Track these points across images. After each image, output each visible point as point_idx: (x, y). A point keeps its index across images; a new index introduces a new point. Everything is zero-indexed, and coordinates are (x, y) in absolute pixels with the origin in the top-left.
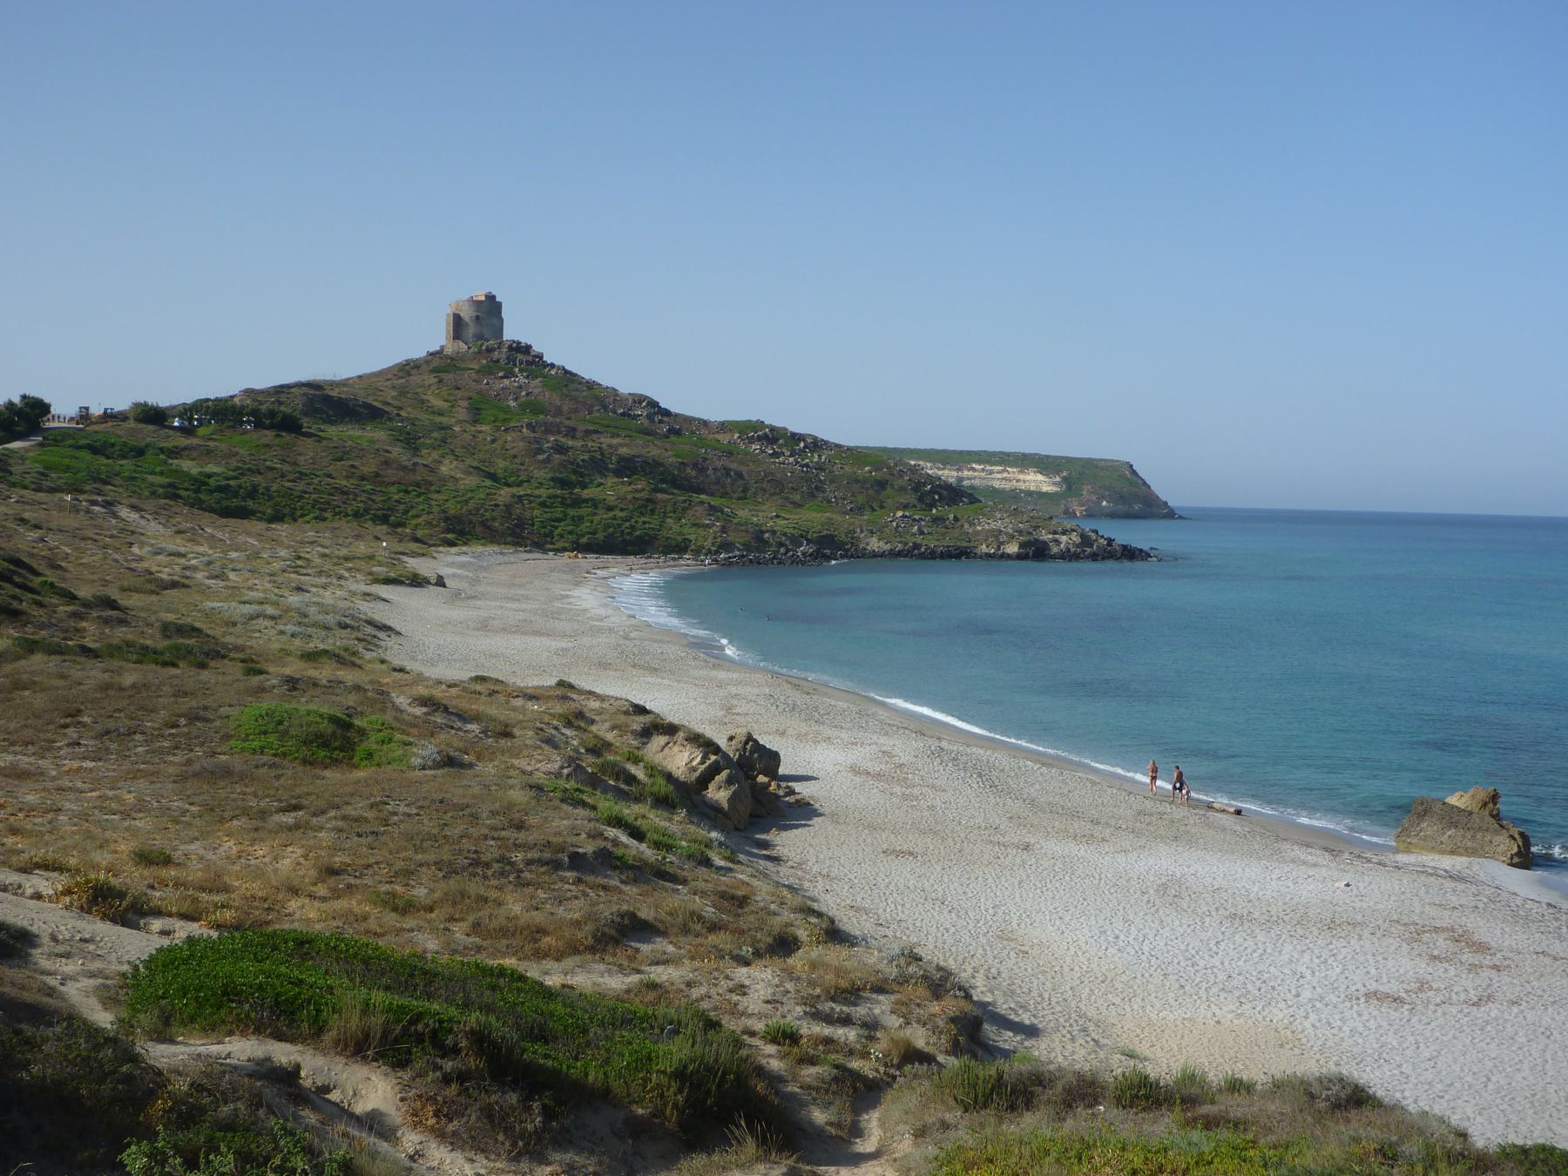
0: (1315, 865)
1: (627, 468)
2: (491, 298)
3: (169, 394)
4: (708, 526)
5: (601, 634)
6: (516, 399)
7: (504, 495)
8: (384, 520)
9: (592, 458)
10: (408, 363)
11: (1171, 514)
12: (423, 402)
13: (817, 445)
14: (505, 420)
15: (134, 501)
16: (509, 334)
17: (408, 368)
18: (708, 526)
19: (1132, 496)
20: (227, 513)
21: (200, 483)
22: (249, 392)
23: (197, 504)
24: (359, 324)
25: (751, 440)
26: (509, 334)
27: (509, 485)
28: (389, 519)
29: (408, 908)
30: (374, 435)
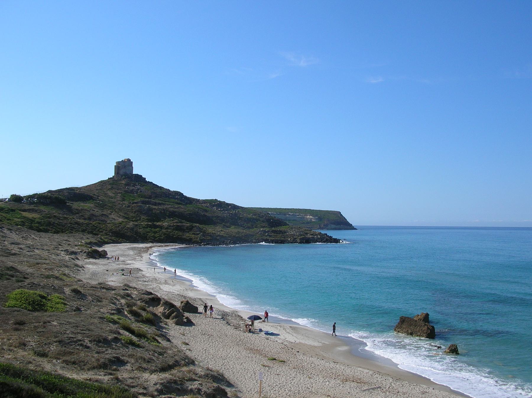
0: (48, 277)
1: (173, 215)
2: (129, 160)
3: (24, 192)
4: (198, 234)
5: (153, 268)
6: (137, 193)
7: (131, 224)
8: (91, 233)
9: (161, 212)
10: (102, 182)
11: (355, 229)
12: (106, 194)
13: (234, 207)
14: (133, 200)
15: (9, 227)
16: (135, 172)
17: (102, 183)
18: (198, 234)
19: (339, 222)
20: (39, 231)
21: (32, 221)
22: (50, 192)
23: (31, 228)
24: (88, 170)
25: (214, 206)
26: (135, 172)
27: (133, 221)
28: (93, 231)
29: (43, 355)
30: (88, 205)
